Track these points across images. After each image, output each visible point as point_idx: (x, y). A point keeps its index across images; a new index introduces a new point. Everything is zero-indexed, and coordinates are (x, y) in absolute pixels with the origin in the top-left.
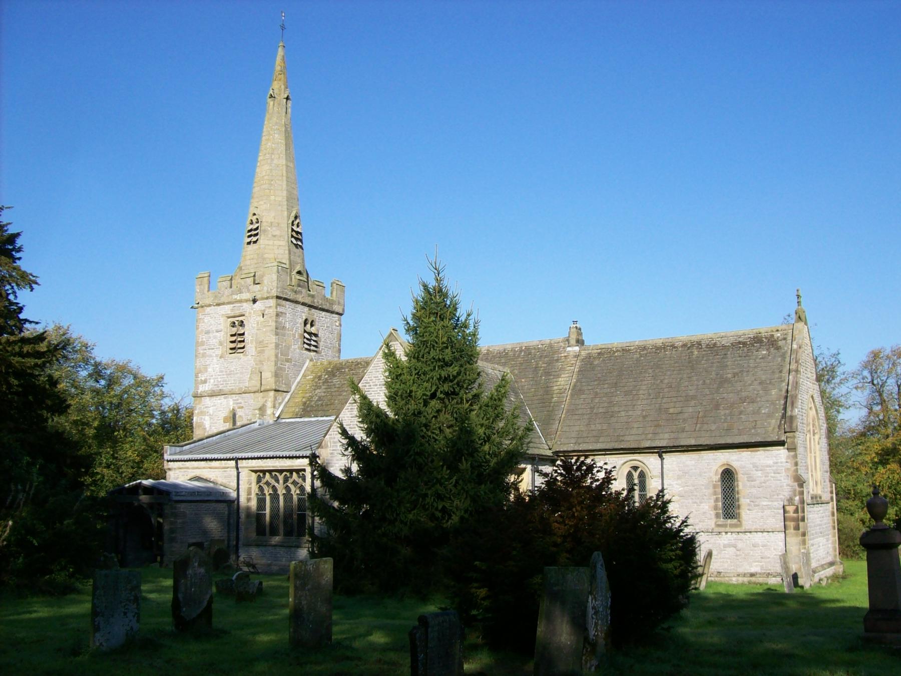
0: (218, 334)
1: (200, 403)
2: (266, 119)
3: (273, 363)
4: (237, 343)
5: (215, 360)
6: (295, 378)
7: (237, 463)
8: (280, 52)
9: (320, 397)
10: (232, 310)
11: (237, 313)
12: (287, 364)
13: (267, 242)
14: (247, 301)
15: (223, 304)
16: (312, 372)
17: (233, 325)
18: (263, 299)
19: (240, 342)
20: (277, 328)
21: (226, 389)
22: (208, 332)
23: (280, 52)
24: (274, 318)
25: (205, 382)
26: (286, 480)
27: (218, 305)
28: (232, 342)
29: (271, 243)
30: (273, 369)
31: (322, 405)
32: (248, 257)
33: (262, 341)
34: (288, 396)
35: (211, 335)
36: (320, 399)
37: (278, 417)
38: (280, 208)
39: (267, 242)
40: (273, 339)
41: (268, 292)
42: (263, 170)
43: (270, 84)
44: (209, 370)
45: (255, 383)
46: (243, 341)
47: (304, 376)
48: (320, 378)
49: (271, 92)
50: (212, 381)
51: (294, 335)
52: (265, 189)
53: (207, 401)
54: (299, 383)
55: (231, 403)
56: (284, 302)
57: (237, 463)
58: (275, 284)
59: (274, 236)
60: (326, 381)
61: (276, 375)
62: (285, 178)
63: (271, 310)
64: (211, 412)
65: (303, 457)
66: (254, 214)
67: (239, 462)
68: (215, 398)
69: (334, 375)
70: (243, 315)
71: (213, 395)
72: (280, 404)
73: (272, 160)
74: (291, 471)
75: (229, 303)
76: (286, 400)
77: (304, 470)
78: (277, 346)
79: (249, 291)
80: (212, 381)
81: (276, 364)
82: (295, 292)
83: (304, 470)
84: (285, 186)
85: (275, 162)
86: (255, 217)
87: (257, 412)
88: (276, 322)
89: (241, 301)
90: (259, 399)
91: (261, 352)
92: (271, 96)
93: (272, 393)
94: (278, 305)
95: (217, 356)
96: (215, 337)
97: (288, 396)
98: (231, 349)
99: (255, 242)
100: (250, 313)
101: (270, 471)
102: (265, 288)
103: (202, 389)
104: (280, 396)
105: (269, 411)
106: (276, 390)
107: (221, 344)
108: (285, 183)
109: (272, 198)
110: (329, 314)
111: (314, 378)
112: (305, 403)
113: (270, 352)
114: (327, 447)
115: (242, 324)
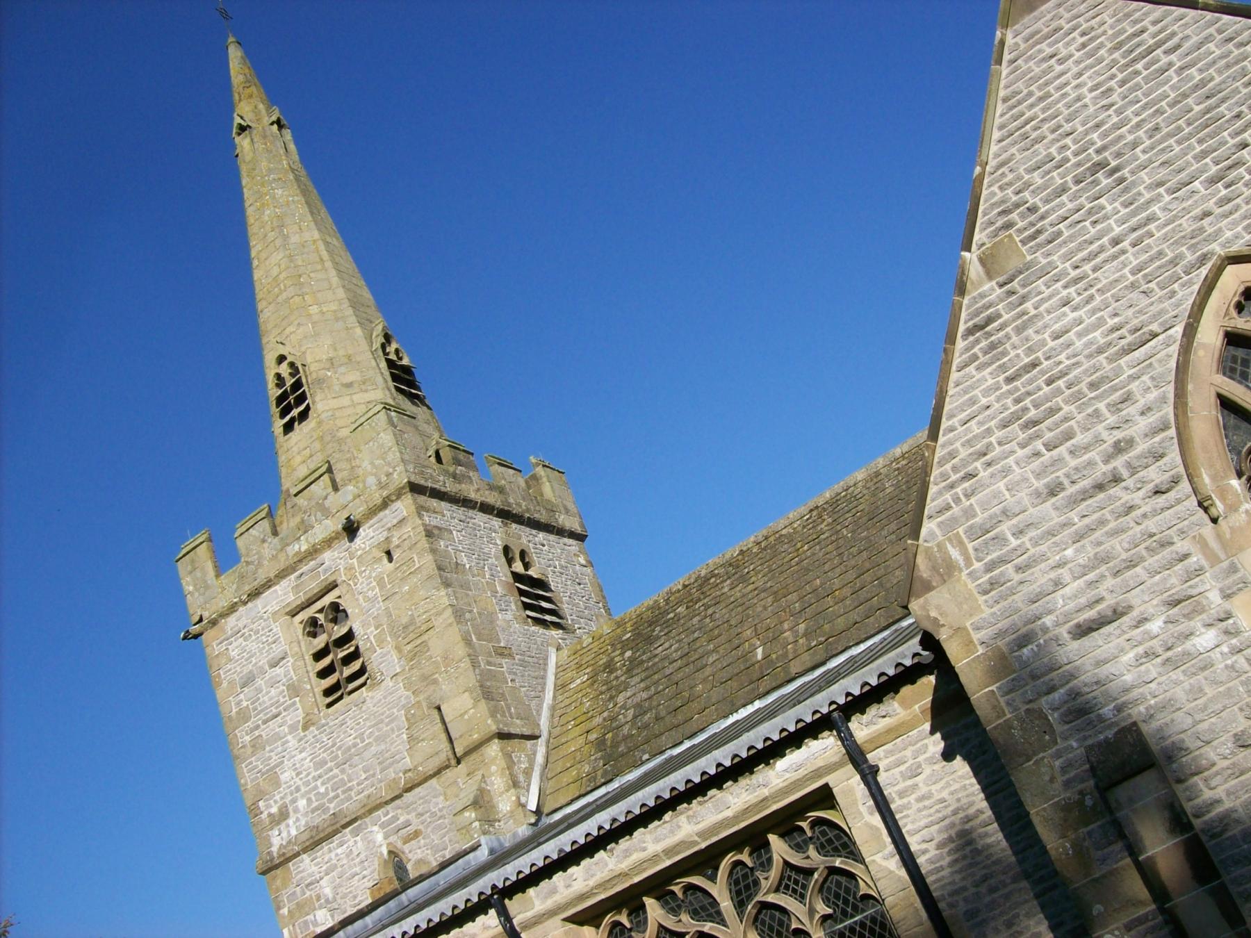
0: (278, 670)
1: (286, 881)
2: (244, 173)
3: (465, 664)
4: (340, 667)
5: (292, 742)
6: (540, 698)
7: (504, 914)
8: (235, 54)
9: (638, 705)
10: (296, 588)
11: (313, 586)
12: (504, 661)
13: (334, 403)
14: (329, 543)
15: (268, 584)
16: (579, 666)
17: (313, 627)
18: (373, 512)
19: (347, 660)
20: (440, 568)
21: (350, 806)
22: (248, 681)
23: (235, 54)
24: (424, 543)
25: (283, 815)
26: (743, 888)
27: (255, 594)
28: (323, 674)
29: (346, 401)
30: (471, 680)
31: (658, 719)
32: (298, 459)
33: (412, 621)
34: (541, 748)
35: (260, 682)
36: (640, 710)
37: (538, 812)
38: (340, 325)
39: (334, 403)
40: (442, 597)
41: (382, 486)
42: (268, 265)
43: (230, 108)
44: (285, 777)
45: (434, 747)
46: (355, 655)
47: (561, 687)
48: (610, 667)
49: (238, 120)
50: (302, 803)
51: (491, 585)
52: (288, 300)
53: (306, 865)
54: (553, 708)
55: (379, 837)
56: (434, 503)
57: (504, 914)
58: (394, 455)
59: (349, 385)
60: (633, 664)
61: (488, 692)
62: (329, 264)
63: (407, 529)
64: (328, 891)
65: (794, 740)
66: (281, 359)
67: (512, 905)
68: (325, 847)
69: (650, 640)
70: (334, 586)
71: (316, 840)
72: (528, 773)
73: (286, 238)
74: (752, 837)
75: (282, 575)
76: (540, 759)
77: (824, 797)
78: (459, 614)
79: (327, 513)
80: (302, 803)
81: (475, 664)
82: (454, 476)
83: (824, 797)
84: (335, 280)
85: (295, 239)
86: (285, 365)
87: (470, 815)
88: (433, 551)
89: (314, 552)
90: (462, 782)
91: (416, 654)
92: (243, 129)
93: (494, 748)
94: (420, 509)
95: (293, 728)
96: (273, 683)
97: (541, 748)
98: (328, 692)
99: (304, 416)
100: (350, 569)
101: (658, 885)
102: (371, 480)
103: (277, 840)
104: (520, 751)
105: (505, 804)
106: (503, 736)
107: (294, 690)
108: (333, 273)
109: (314, 309)
110: (552, 537)
111: (593, 678)
112: (600, 743)
113: (446, 639)
114: (947, 570)
115: (337, 612)
